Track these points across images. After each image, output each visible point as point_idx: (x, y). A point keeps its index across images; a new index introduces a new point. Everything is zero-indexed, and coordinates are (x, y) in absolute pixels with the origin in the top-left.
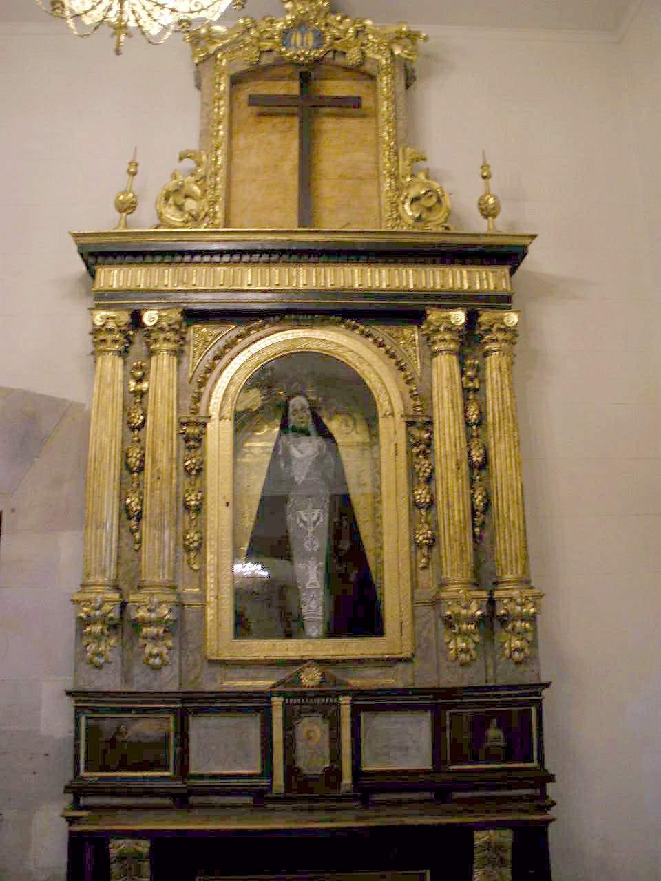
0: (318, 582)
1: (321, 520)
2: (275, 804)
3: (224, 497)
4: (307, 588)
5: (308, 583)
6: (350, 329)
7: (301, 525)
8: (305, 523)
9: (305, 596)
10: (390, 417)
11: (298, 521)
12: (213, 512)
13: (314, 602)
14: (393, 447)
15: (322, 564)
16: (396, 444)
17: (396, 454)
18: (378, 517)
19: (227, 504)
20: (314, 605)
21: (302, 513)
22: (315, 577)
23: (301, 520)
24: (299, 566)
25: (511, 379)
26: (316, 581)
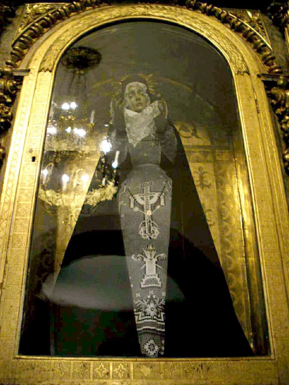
0: (158, 279)
1: (162, 203)
2: (100, 358)
3: (31, 151)
4: (143, 286)
5: (144, 280)
6: (159, 196)
7: (136, 209)
8: (142, 207)
9: (138, 298)
10: (246, 74)
11: (132, 205)
12: (11, 177)
13: (152, 305)
14: (253, 103)
15: (164, 255)
16: (256, 101)
17: (258, 112)
18: (225, 221)
19: (34, 159)
20: (152, 309)
21: (138, 197)
22: (154, 272)
23: (136, 203)
24: (132, 259)
25: (250, 291)
26: (157, 277)
